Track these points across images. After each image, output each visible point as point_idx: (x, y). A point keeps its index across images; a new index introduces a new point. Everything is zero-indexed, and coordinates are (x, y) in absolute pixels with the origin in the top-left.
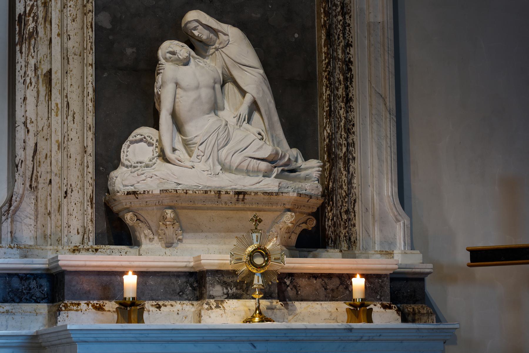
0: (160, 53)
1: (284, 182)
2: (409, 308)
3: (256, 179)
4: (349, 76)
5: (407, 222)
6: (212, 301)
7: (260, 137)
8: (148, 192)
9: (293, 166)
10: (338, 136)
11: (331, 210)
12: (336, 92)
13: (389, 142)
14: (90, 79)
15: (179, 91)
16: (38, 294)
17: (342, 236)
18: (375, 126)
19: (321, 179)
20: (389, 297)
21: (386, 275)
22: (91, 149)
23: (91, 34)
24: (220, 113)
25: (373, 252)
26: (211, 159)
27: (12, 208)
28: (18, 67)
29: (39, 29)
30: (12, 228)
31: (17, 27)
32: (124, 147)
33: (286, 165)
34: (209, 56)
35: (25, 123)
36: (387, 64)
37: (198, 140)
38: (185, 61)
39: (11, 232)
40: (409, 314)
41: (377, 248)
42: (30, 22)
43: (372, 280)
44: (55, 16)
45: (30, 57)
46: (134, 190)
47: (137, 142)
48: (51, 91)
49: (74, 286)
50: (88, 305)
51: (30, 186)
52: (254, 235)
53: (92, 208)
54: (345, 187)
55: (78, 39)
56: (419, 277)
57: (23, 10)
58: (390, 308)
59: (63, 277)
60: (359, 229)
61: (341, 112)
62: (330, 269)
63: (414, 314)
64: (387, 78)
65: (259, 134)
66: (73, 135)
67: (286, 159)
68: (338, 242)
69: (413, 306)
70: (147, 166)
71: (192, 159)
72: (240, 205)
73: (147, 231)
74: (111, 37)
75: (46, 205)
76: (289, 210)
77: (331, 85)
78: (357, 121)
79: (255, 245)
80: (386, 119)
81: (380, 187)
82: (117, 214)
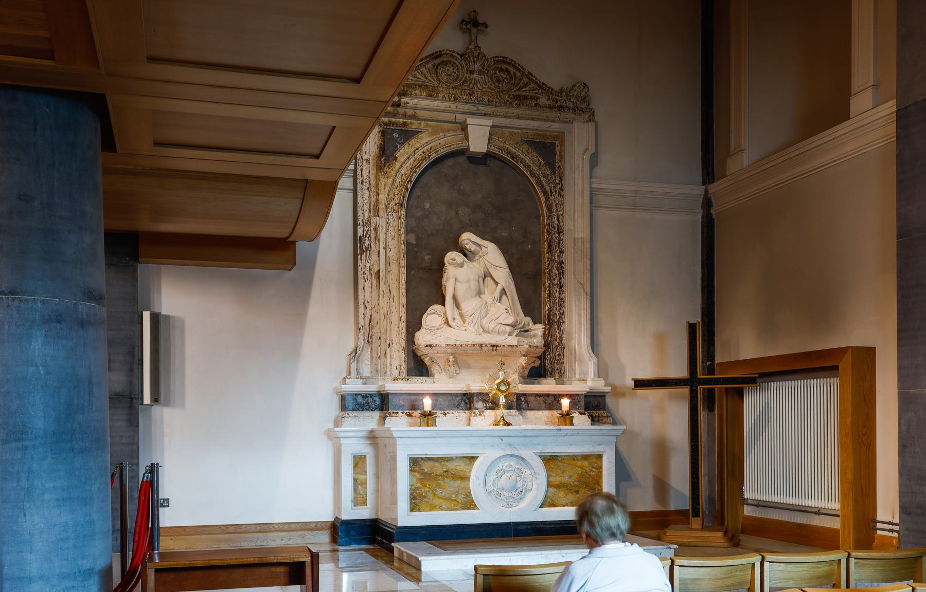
0: (446, 260)
1: (521, 339)
2: (596, 413)
3: (504, 337)
4: (561, 271)
5: (596, 361)
6: (477, 411)
7: (506, 311)
8: (439, 345)
9: (527, 328)
10: (554, 309)
11: (549, 354)
12: (553, 282)
13: (585, 313)
14: (404, 276)
15: (457, 283)
16: (373, 406)
17: (556, 369)
18: (577, 302)
19: (544, 336)
20: (584, 408)
21: (582, 394)
22: (404, 319)
23: (404, 248)
24: (482, 296)
25: (574, 379)
26: (476, 326)
27: (357, 354)
28: (359, 269)
29: (372, 244)
30: (357, 367)
31: (359, 244)
32: (424, 317)
33: (522, 328)
34: (475, 260)
35: (364, 303)
36: (585, 264)
37: (469, 313)
38: (461, 265)
39: (357, 369)
40: (595, 417)
41: (577, 377)
42: (367, 240)
43: (573, 398)
44: (381, 236)
45: (367, 262)
46: (430, 344)
47: (431, 314)
48: (379, 283)
49: (395, 402)
50: (403, 413)
51: (368, 341)
52: (500, 373)
53: (405, 354)
54: (558, 340)
55: (396, 250)
56: (603, 394)
57: (362, 233)
58: (584, 414)
59: (388, 397)
60: (566, 365)
61: (556, 294)
62: (548, 391)
63: (599, 416)
64: (585, 273)
65: (506, 309)
66: (393, 309)
67: (523, 324)
68: (553, 373)
69: (598, 412)
70: (438, 329)
71: (465, 325)
72: (494, 352)
73: (438, 368)
74: (415, 249)
75: (377, 352)
76: (524, 356)
77: (550, 278)
78: (566, 300)
79: (501, 378)
80: (584, 298)
81: (580, 340)
82: (420, 357)
